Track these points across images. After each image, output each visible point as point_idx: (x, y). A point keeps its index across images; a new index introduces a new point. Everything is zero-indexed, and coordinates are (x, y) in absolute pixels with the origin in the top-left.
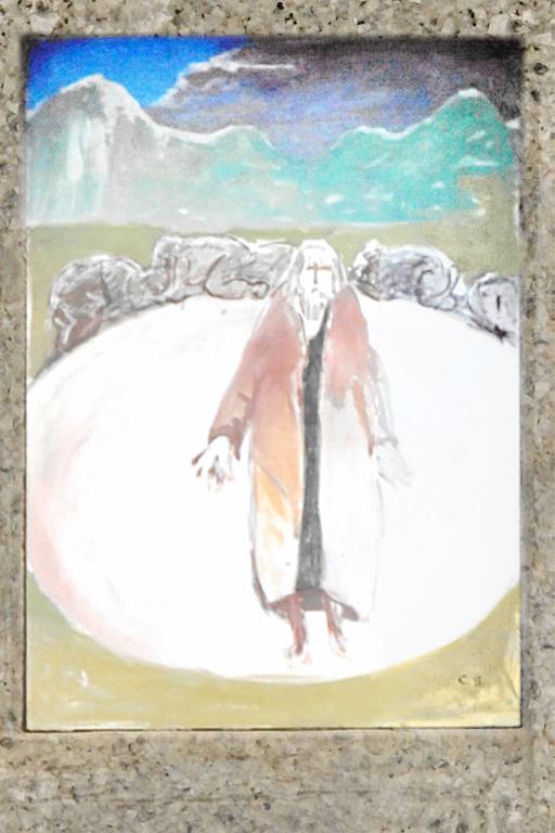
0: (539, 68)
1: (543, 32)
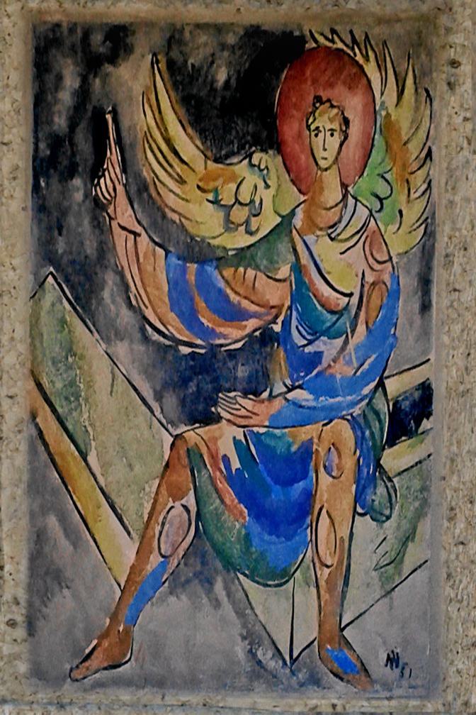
0: (12, 624)
1: (10, 655)
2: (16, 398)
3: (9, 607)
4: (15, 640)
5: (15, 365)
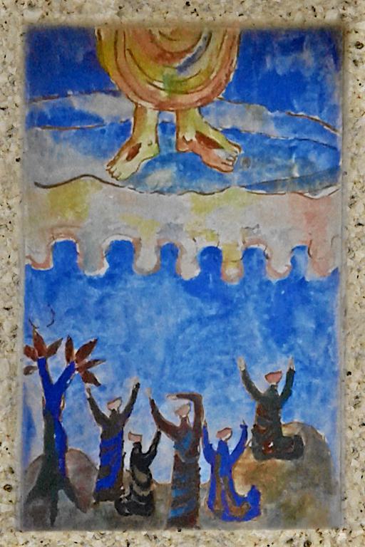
2: (129, 541)
3: (6, 475)
4: (321, 542)
5: (10, 283)
